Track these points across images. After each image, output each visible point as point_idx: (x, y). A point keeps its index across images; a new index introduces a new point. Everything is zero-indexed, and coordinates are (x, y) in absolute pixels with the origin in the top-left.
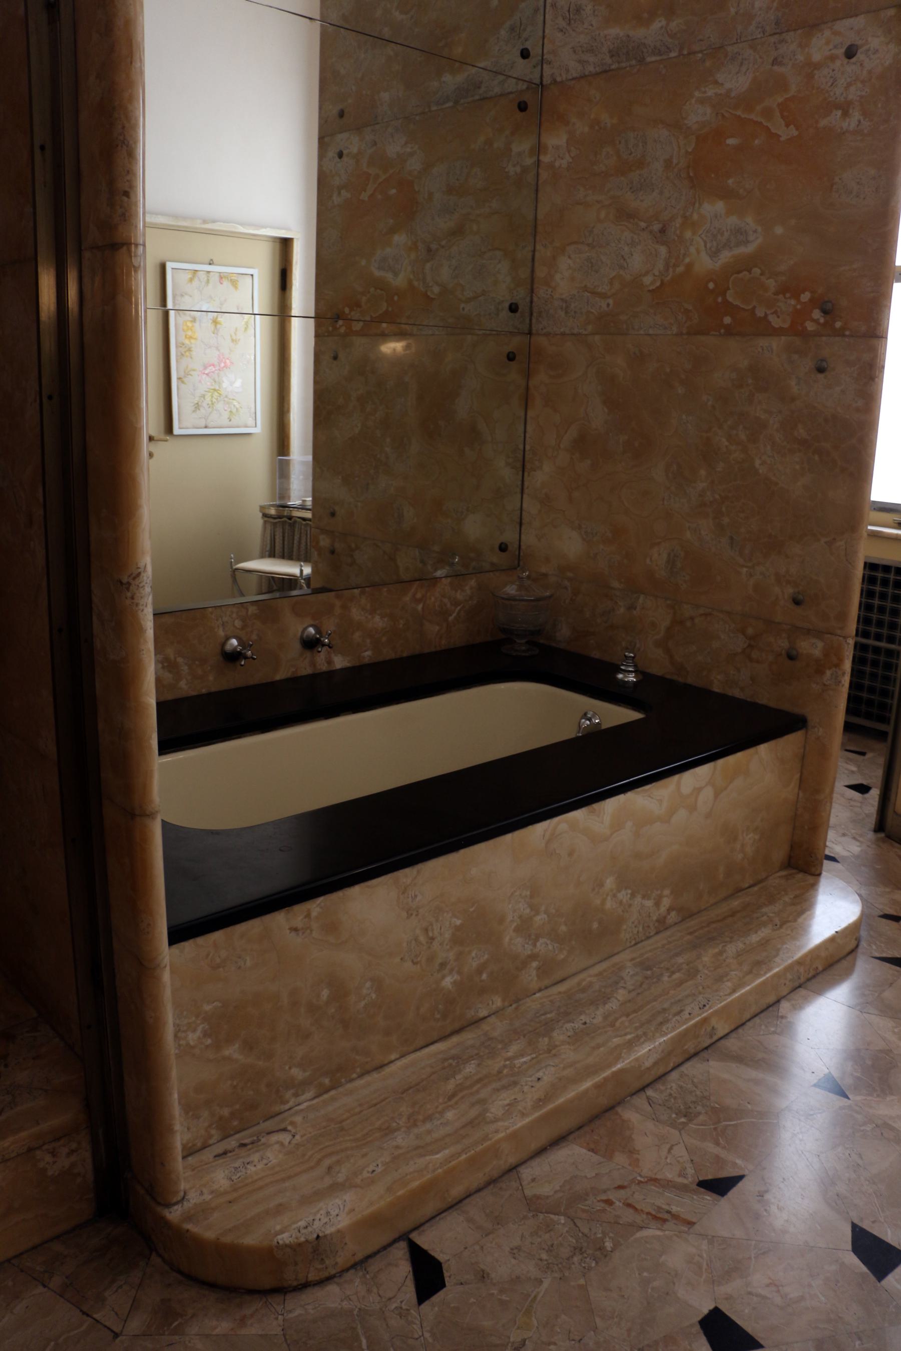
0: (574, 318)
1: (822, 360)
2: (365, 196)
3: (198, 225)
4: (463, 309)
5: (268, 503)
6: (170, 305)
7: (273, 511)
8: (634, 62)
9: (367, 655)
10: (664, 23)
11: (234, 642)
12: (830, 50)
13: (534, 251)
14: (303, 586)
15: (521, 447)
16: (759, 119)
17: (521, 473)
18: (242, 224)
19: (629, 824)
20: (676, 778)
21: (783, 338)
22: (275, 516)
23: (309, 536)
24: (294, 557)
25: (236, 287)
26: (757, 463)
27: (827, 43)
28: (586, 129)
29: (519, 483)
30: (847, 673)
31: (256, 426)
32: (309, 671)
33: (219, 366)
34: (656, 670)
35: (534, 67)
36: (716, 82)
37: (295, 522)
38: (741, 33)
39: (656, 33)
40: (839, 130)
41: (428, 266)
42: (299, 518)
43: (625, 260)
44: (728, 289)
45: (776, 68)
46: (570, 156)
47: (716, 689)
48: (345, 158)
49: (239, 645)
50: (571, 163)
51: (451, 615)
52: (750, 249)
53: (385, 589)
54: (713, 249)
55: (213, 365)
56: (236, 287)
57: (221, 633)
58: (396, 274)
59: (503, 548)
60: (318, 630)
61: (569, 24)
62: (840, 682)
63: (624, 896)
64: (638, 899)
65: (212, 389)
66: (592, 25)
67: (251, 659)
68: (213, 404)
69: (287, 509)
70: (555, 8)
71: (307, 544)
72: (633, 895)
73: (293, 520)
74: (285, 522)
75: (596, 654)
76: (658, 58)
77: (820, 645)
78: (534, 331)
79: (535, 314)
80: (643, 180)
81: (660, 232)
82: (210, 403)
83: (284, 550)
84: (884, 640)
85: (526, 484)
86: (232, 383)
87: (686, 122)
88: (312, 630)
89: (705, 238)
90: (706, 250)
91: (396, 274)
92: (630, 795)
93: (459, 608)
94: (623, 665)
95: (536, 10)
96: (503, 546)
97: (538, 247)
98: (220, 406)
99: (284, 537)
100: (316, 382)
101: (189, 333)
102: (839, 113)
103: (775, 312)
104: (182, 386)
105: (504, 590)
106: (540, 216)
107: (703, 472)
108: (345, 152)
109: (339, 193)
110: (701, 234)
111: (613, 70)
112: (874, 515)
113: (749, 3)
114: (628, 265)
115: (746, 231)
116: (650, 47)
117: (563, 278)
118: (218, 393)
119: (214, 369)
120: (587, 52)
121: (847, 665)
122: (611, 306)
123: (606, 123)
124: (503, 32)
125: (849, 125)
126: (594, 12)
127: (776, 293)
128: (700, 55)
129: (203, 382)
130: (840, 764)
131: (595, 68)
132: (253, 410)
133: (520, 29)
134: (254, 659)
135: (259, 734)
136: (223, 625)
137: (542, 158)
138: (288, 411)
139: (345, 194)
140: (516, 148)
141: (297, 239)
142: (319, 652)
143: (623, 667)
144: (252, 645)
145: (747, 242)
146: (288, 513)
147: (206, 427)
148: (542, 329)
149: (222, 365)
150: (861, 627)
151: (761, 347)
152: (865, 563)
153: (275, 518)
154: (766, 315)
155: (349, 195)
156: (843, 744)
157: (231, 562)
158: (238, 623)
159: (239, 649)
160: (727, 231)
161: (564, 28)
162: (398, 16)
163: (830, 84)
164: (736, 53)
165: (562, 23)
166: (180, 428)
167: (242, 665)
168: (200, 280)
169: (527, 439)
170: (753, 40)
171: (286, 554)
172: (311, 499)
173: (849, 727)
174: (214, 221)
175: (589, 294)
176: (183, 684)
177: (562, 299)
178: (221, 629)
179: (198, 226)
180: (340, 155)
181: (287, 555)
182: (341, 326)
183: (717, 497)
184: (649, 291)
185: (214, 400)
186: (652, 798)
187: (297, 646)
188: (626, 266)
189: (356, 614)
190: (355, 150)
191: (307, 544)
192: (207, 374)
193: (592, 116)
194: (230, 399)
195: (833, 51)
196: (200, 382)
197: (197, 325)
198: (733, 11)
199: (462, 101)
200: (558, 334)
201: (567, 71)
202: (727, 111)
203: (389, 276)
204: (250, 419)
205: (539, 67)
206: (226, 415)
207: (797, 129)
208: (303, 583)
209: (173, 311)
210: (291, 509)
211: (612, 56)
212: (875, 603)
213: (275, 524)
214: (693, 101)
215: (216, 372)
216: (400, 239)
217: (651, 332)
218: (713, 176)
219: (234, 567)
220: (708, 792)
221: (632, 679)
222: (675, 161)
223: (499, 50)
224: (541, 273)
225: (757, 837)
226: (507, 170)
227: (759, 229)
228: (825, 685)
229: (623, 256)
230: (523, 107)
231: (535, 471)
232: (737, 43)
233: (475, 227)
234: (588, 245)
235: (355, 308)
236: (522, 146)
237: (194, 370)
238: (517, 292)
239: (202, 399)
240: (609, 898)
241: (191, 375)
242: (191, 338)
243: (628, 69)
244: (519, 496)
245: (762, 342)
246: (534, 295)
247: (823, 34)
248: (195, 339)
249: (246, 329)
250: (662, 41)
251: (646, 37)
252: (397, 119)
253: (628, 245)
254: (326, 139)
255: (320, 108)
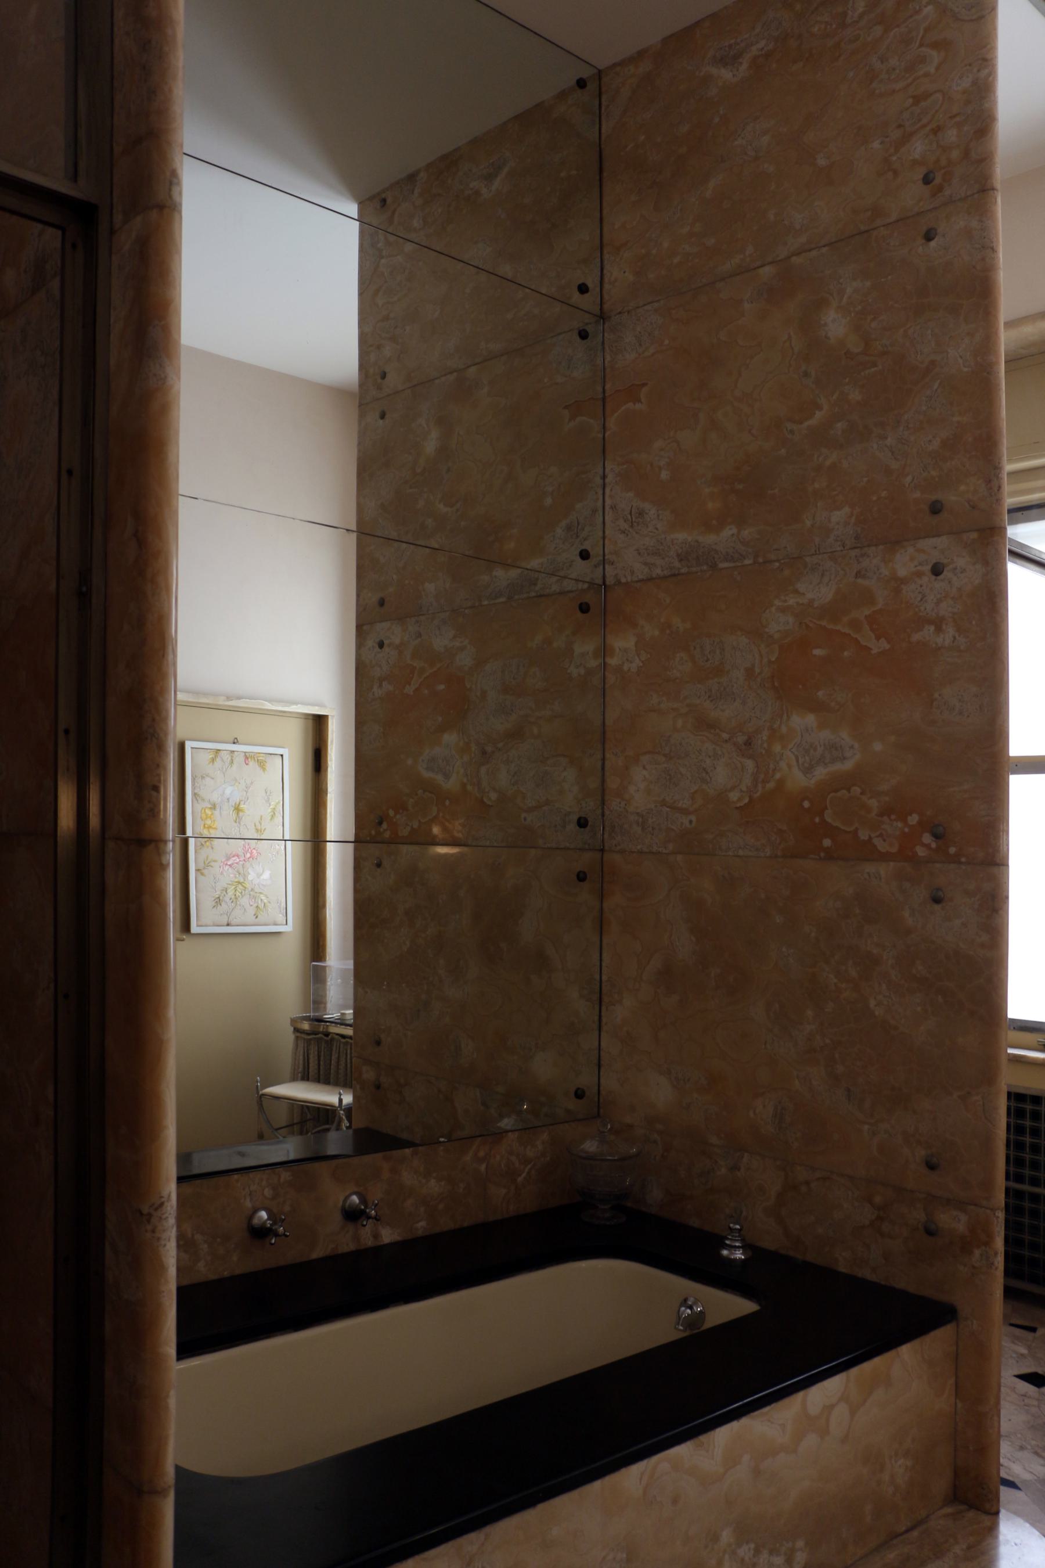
0: (653, 835)
1: (938, 889)
2: (409, 690)
3: (222, 702)
4: (525, 819)
5: (301, 1015)
6: (189, 832)
7: (306, 1026)
8: (705, 567)
9: (421, 1227)
10: (735, 531)
11: (264, 1214)
12: (916, 566)
13: (603, 759)
14: (342, 1118)
15: (597, 977)
16: (847, 630)
17: (597, 1007)
18: (270, 701)
19: (746, 1458)
20: (800, 1395)
21: (892, 864)
22: (309, 1032)
23: (349, 1056)
24: (332, 1081)
25: (264, 769)
26: (872, 1003)
27: (912, 559)
28: (657, 633)
29: (596, 1018)
30: (1000, 1252)
31: (286, 924)
32: (352, 1247)
33: (245, 856)
34: (768, 1243)
35: (596, 566)
36: (796, 592)
37: (332, 1039)
38: (819, 544)
39: (727, 541)
40: (934, 645)
41: (483, 770)
42: (337, 1034)
43: (707, 773)
44: (826, 808)
45: (860, 581)
46: (640, 660)
47: (842, 1269)
48: (386, 649)
49: (269, 1219)
50: (641, 667)
51: (520, 1175)
52: (848, 765)
53: (442, 1148)
54: (806, 765)
55: (238, 856)
56: (264, 769)
57: (248, 1204)
58: (447, 776)
59: (579, 1094)
60: (363, 1200)
61: (632, 526)
62: (993, 1264)
63: (745, 1551)
64: (765, 1555)
65: (236, 882)
66: (657, 529)
67: (283, 1237)
68: (236, 898)
69: (323, 1023)
70: (614, 509)
71: (346, 1065)
72: (757, 1551)
73: (330, 1037)
74: (321, 1039)
75: (695, 1222)
76: (732, 565)
77: (964, 1218)
78: (606, 848)
79: (607, 829)
80: (722, 689)
81: (745, 744)
82: (233, 897)
83: (319, 1068)
84: (1042, 1186)
85: (604, 1020)
86: (259, 875)
87: (767, 630)
88: (355, 1199)
89: (796, 753)
90: (798, 765)
91: (447, 776)
92: (745, 1421)
93: (529, 1166)
94: (728, 1239)
95: (594, 511)
96: (581, 875)
97: (608, 755)
98: (244, 901)
99: (319, 1056)
100: (356, 891)
101: (208, 822)
102: (932, 628)
103: (881, 835)
104: (201, 878)
105: (582, 1147)
106: (609, 722)
107: (810, 1013)
108: (386, 642)
109: (380, 686)
110: (792, 749)
111: (683, 574)
112: (1013, 1035)
113: (825, 518)
114: (711, 779)
115: (841, 746)
116: (721, 553)
117: (638, 791)
118: (243, 886)
119: (238, 860)
120: (653, 554)
121: (999, 1244)
122: (694, 824)
123: (678, 628)
124: (559, 531)
125: (944, 640)
126: (658, 516)
127: (881, 814)
128: (777, 564)
129: (225, 874)
130: (1004, 1343)
131: (662, 571)
132: (283, 904)
133: (577, 528)
134: (287, 1236)
135: (290, 1332)
136: (250, 1194)
137: (609, 661)
138: (324, 906)
139: (387, 687)
140: (578, 649)
141: (333, 716)
142: (364, 1226)
143: (728, 1242)
144: (284, 1219)
145: (844, 759)
146: (324, 1028)
147: (228, 925)
148: (616, 846)
149: (248, 855)
150: (1012, 1169)
151: (868, 873)
152: (1009, 1094)
153: (308, 1034)
154: (870, 838)
155: (391, 688)
156: (1006, 1317)
157: (257, 1086)
158: (268, 1192)
159: (269, 1223)
160: (820, 746)
161: (626, 529)
162: (442, 508)
163: (919, 599)
164: (816, 564)
165: (625, 526)
166: (198, 926)
167: (272, 1244)
168: (223, 760)
169: (604, 968)
170: (831, 552)
171: (321, 1077)
172: (352, 1011)
173: (1009, 1293)
174: (239, 698)
175: (668, 809)
176: (201, 1266)
177: (638, 814)
178: (248, 1200)
179: (221, 703)
180: (381, 645)
181: (323, 1078)
182: (385, 830)
183: (828, 1041)
184: (737, 808)
185: (238, 894)
186: (772, 1423)
187: (338, 1217)
188: (709, 779)
189: (408, 1178)
190: (397, 641)
191: (346, 1065)
192: (230, 866)
193: (662, 620)
194: (256, 893)
195: (919, 568)
196: (222, 873)
197: (217, 812)
198: (808, 523)
199: (516, 597)
200: (634, 852)
201: (632, 573)
202: (811, 621)
203: (439, 778)
204: (281, 915)
205: (602, 567)
206: (251, 911)
207: (889, 642)
208: (343, 1115)
209: (193, 839)
210: (328, 1024)
211: (681, 560)
212: (1030, 1122)
213: (309, 1042)
214: (773, 609)
215: (241, 863)
216: (450, 738)
217: (741, 853)
218: (800, 687)
219: (261, 1093)
220: (841, 1411)
221: (740, 1256)
222: (757, 670)
223: (556, 548)
224: (613, 783)
225: (909, 1463)
226: (569, 671)
227: (856, 745)
228: (974, 1267)
229: (704, 769)
230: (584, 608)
231: (615, 1005)
232: (816, 554)
233: (535, 731)
234: (665, 755)
235: (401, 811)
236: (585, 647)
237: (215, 861)
238: (586, 803)
239: (225, 893)
240: (727, 1556)
241: (212, 867)
242: (210, 827)
243: (699, 574)
244: (596, 1033)
245: (869, 868)
246: (605, 807)
247: (906, 551)
248: (215, 829)
249: (272, 817)
250: (734, 548)
251: (716, 544)
252: (444, 612)
253: (710, 757)
254: (365, 628)
255: (358, 595)
